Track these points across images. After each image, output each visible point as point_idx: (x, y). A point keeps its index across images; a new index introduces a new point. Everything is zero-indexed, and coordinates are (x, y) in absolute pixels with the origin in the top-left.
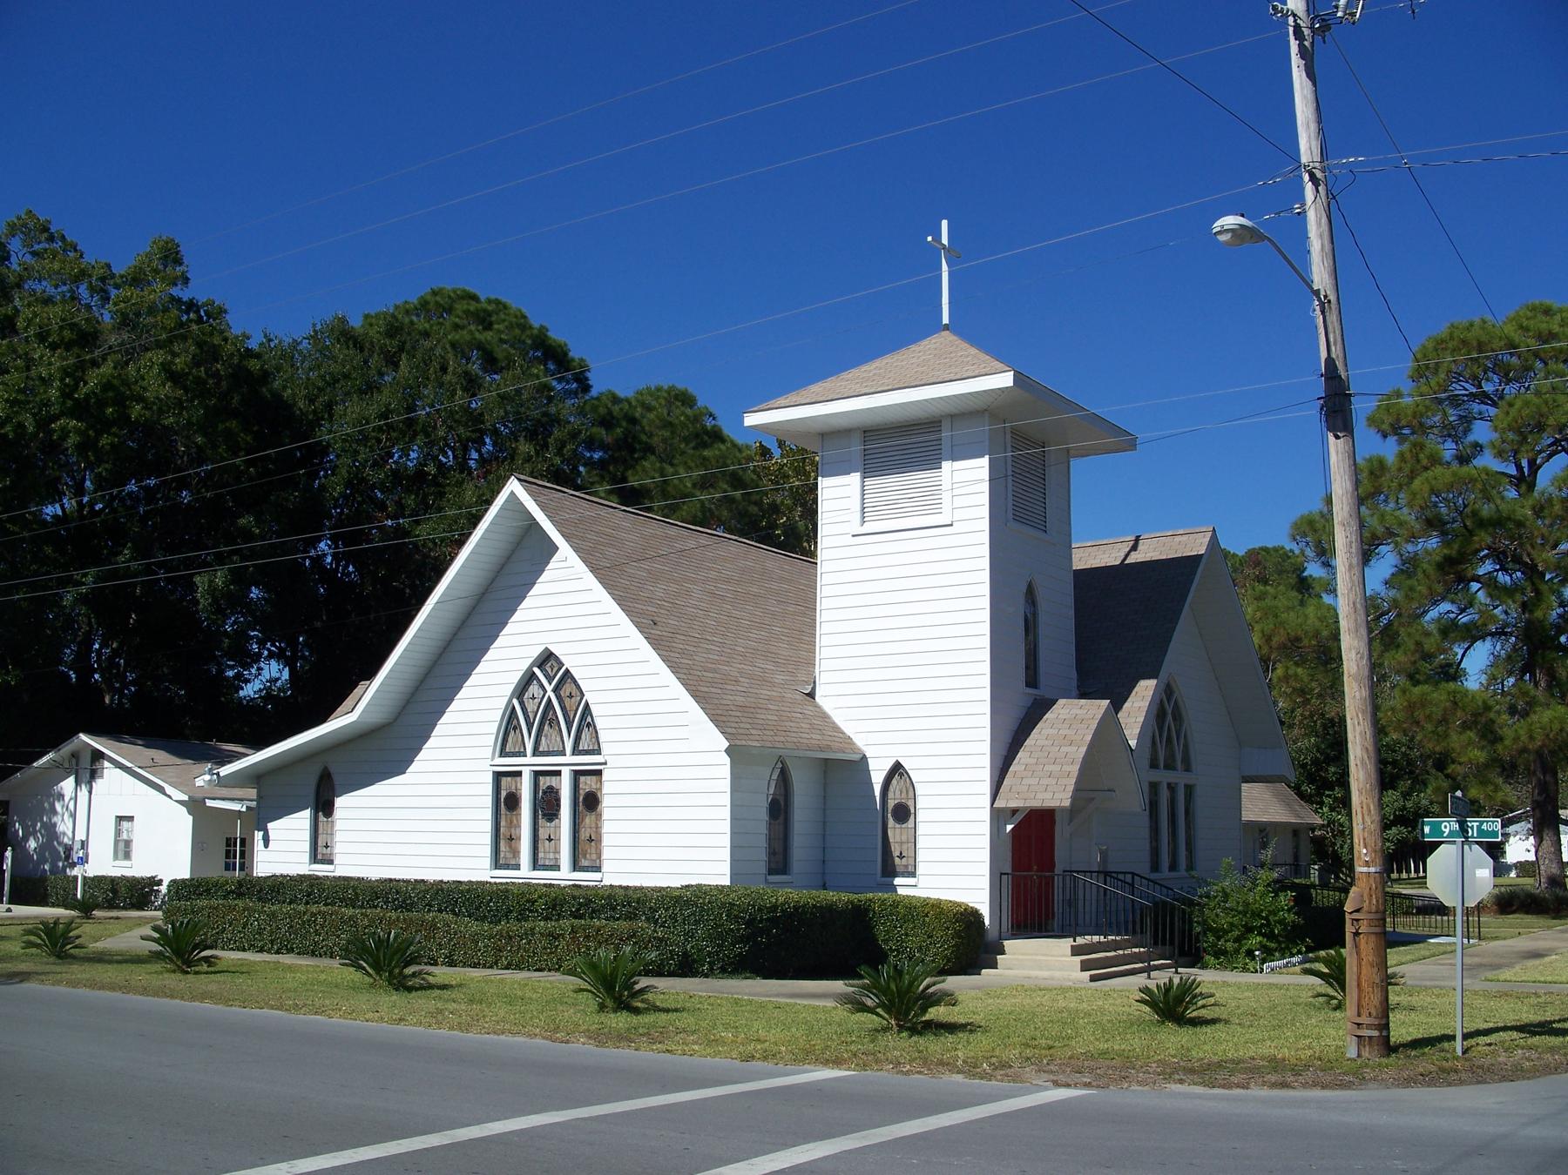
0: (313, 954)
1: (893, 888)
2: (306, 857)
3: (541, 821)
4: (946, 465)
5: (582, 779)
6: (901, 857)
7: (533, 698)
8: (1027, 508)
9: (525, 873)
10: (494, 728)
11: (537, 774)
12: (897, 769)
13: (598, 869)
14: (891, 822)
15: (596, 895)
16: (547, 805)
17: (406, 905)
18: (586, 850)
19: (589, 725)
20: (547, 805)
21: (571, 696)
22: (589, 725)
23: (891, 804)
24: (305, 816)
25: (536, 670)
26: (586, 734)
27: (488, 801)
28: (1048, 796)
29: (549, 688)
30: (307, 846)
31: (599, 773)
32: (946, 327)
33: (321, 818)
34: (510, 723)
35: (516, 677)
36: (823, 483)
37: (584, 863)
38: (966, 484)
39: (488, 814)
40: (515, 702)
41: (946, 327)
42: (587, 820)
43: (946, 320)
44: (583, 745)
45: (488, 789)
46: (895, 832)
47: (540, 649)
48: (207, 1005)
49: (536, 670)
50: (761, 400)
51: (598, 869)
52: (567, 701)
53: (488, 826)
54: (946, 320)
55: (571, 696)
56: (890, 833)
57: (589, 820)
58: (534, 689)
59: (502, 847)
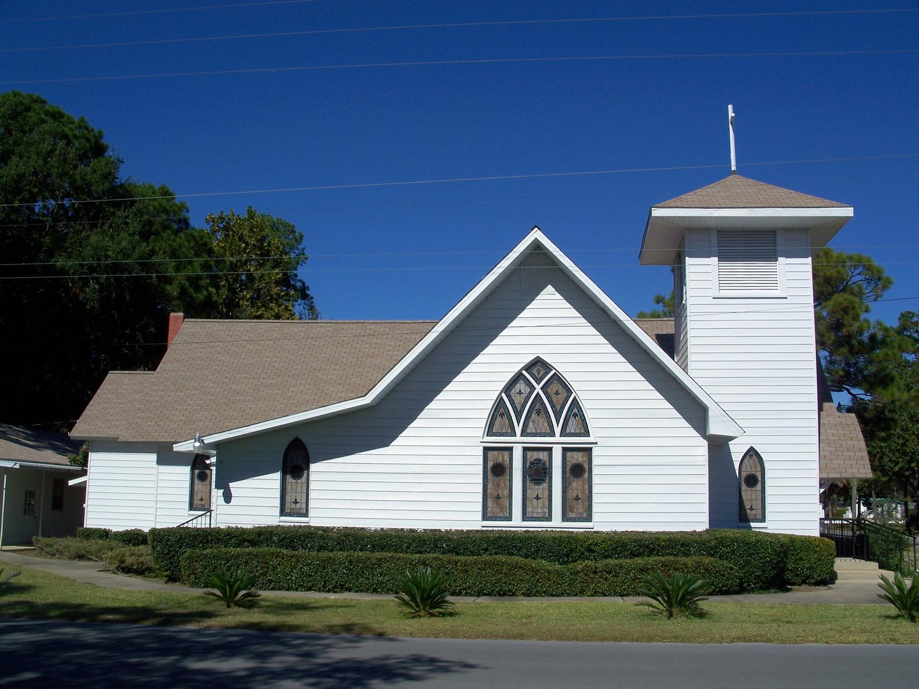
0: (375, 591)
1: (750, 528)
2: (277, 511)
3: (196, 481)
4: (781, 260)
5: (569, 454)
6: (751, 509)
7: (520, 393)
8: (832, 292)
9: (517, 523)
10: (485, 414)
11: (525, 450)
12: (752, 453)
13: (306, 515)
14: (744, 487)
15: (658, 539)
16: (537, 472)
17: (455, 550)
18: (579, 503)
19: (575, 415)
20: (537, 472)
21: (557, 393)
22: (575, 415)
23: (744, 474)
24: (273, 481)
25: (524, 372)
26: (572, 422)
27: (480, 469)
28: (856, 471)
29: (538, 388)
30: (187, 499)
31: (590, 449)
32: (734, 172)
33: (289, 479)
34: (499, 409)
35: (509, 377)
36: (689, 261)
37: (571, 515)
38: (795, 275)
39: (480, 479)
40: (503, 395)
41: (734, 172)
42: (574, 484)
43: (733, 168)
44: (571, 428)
45: (480, 460)
46: (748, 494)
47: (535, 356)
48: (479, 640)
49: (524, 372)
50: (665, 196)
51: (306, 515)
52: (554, 398)
53: (480, 489)
54: (733, 168)
55: (557, 393)
56: (743, 494)
57: (576, 484)
58: (521, 386)
59: (494, 502)
